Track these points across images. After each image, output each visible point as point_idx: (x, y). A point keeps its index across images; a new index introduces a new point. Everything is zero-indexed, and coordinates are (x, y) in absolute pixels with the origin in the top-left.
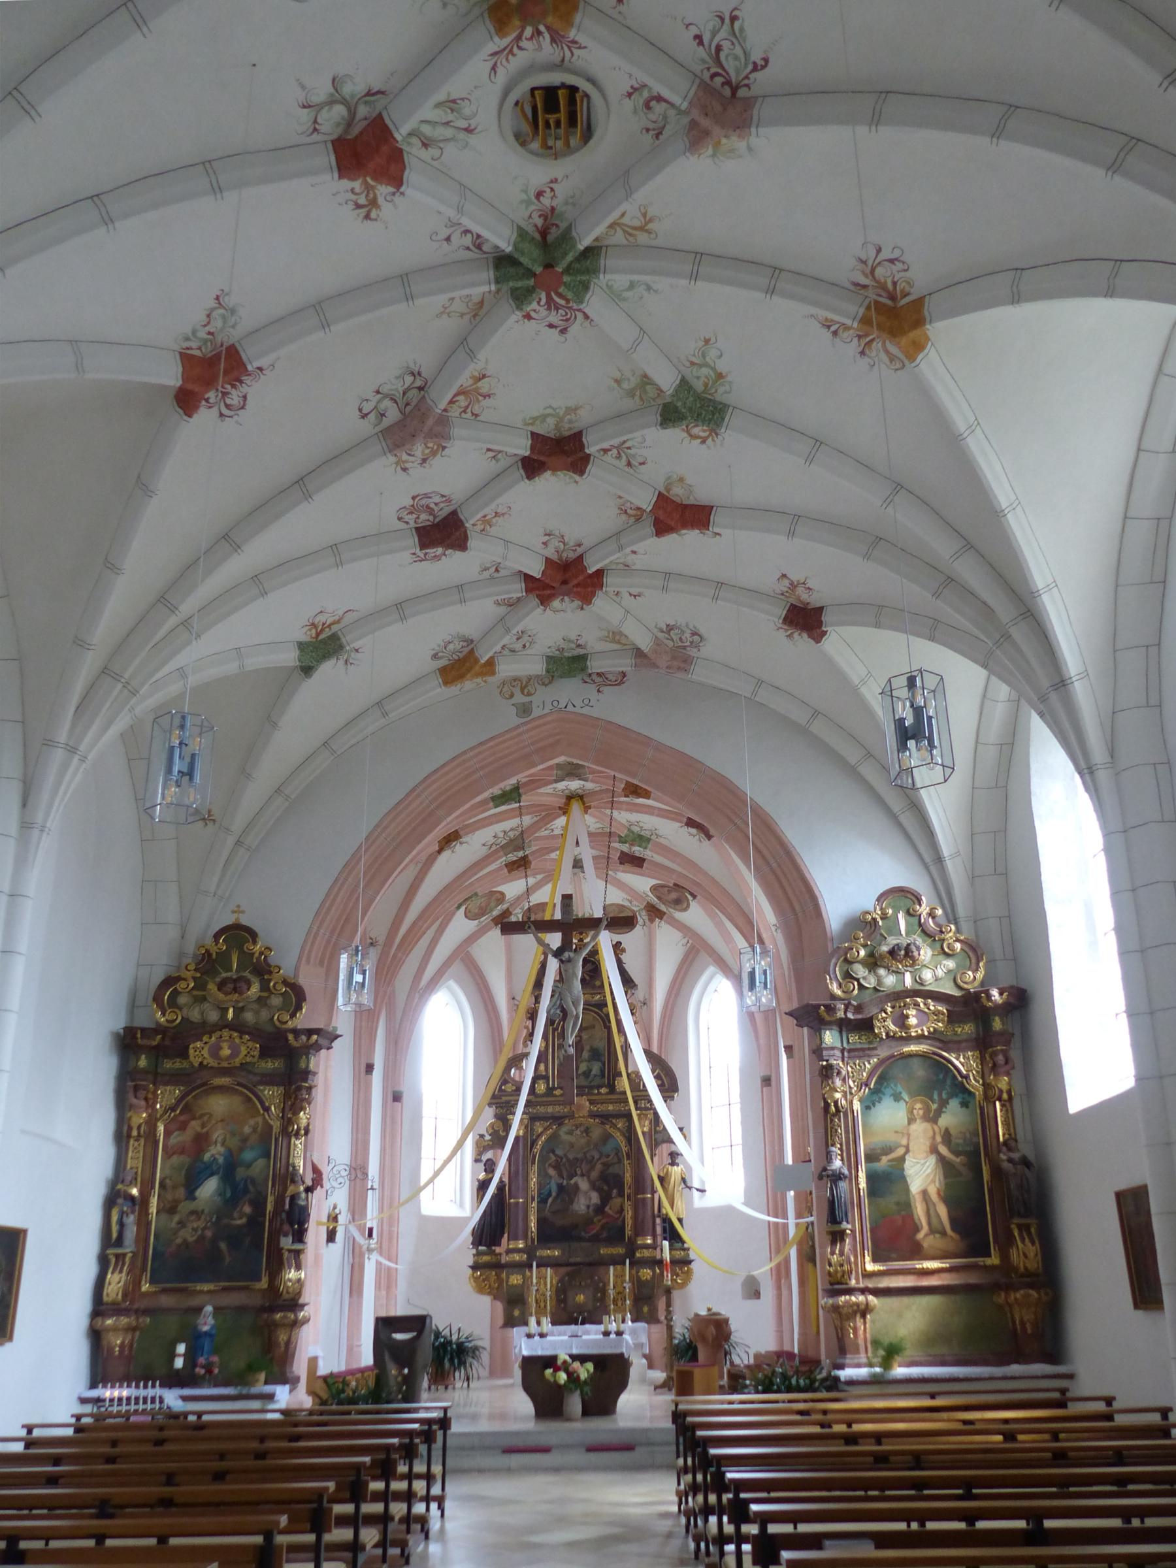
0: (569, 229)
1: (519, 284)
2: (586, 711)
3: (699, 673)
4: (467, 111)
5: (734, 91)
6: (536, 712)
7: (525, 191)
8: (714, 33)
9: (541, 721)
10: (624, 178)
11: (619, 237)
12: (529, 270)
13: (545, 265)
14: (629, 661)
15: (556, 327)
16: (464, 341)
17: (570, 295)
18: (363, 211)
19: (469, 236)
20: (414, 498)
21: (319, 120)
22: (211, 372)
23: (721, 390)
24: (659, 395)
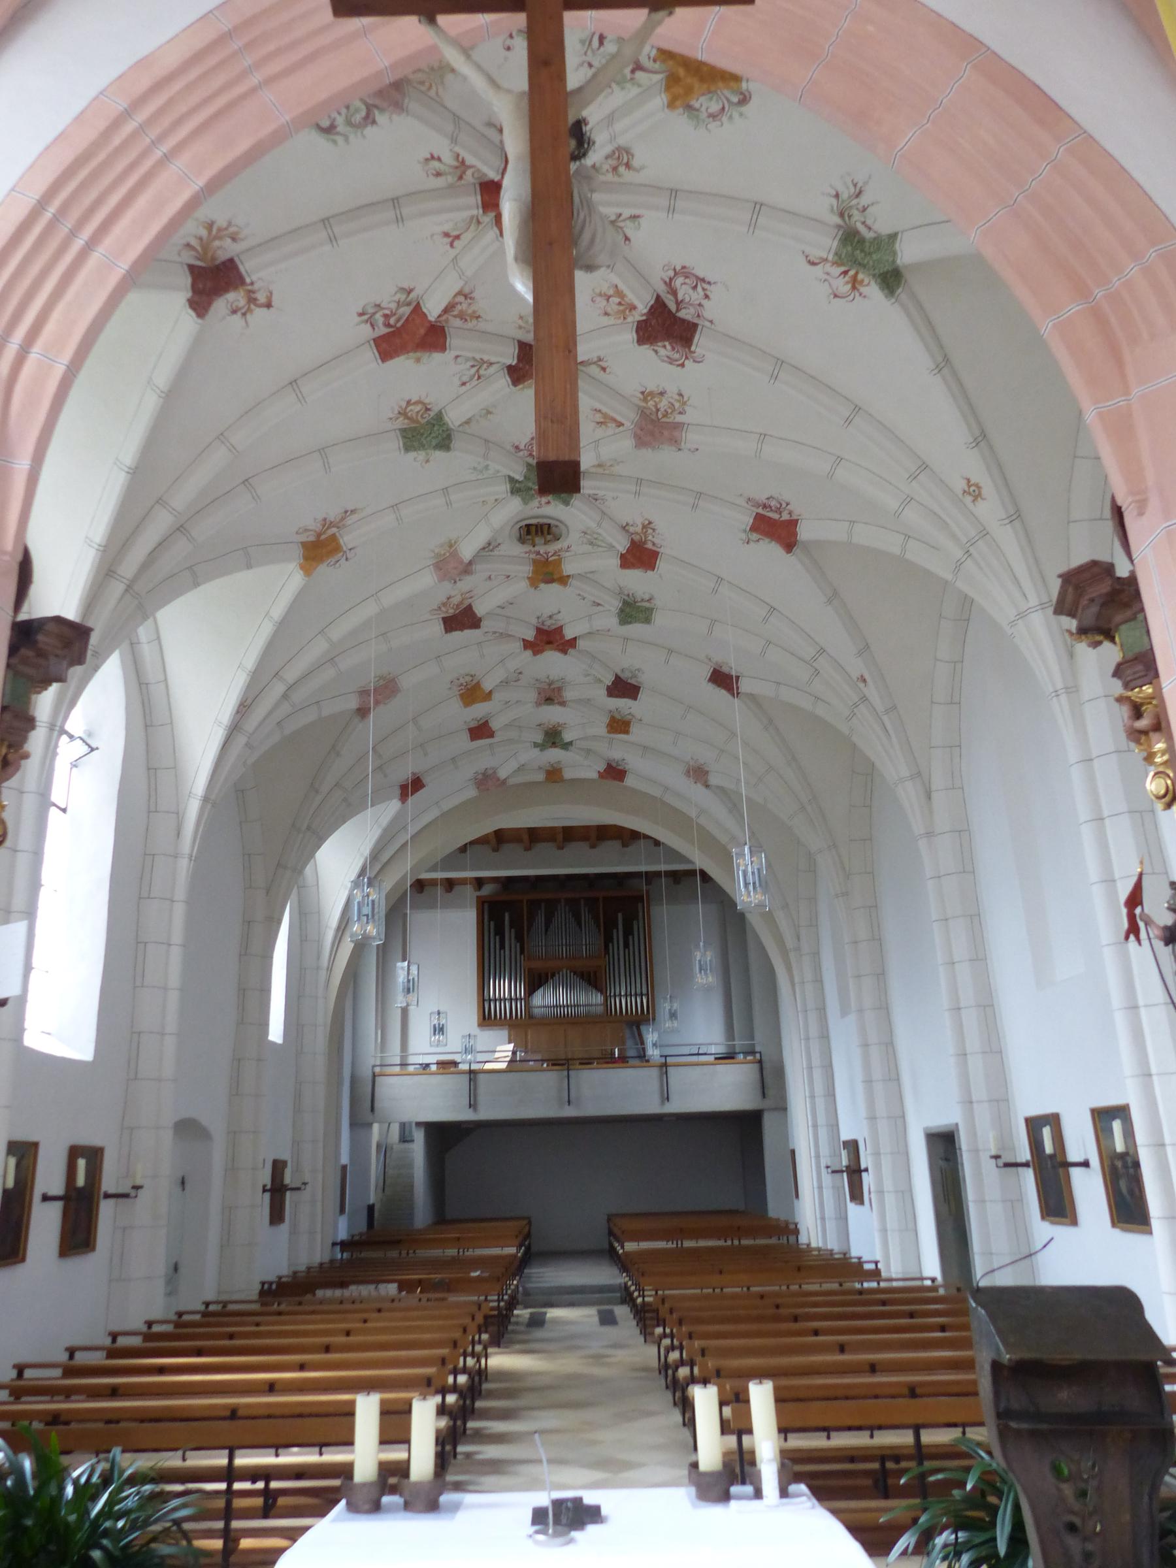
20: (683, 365)
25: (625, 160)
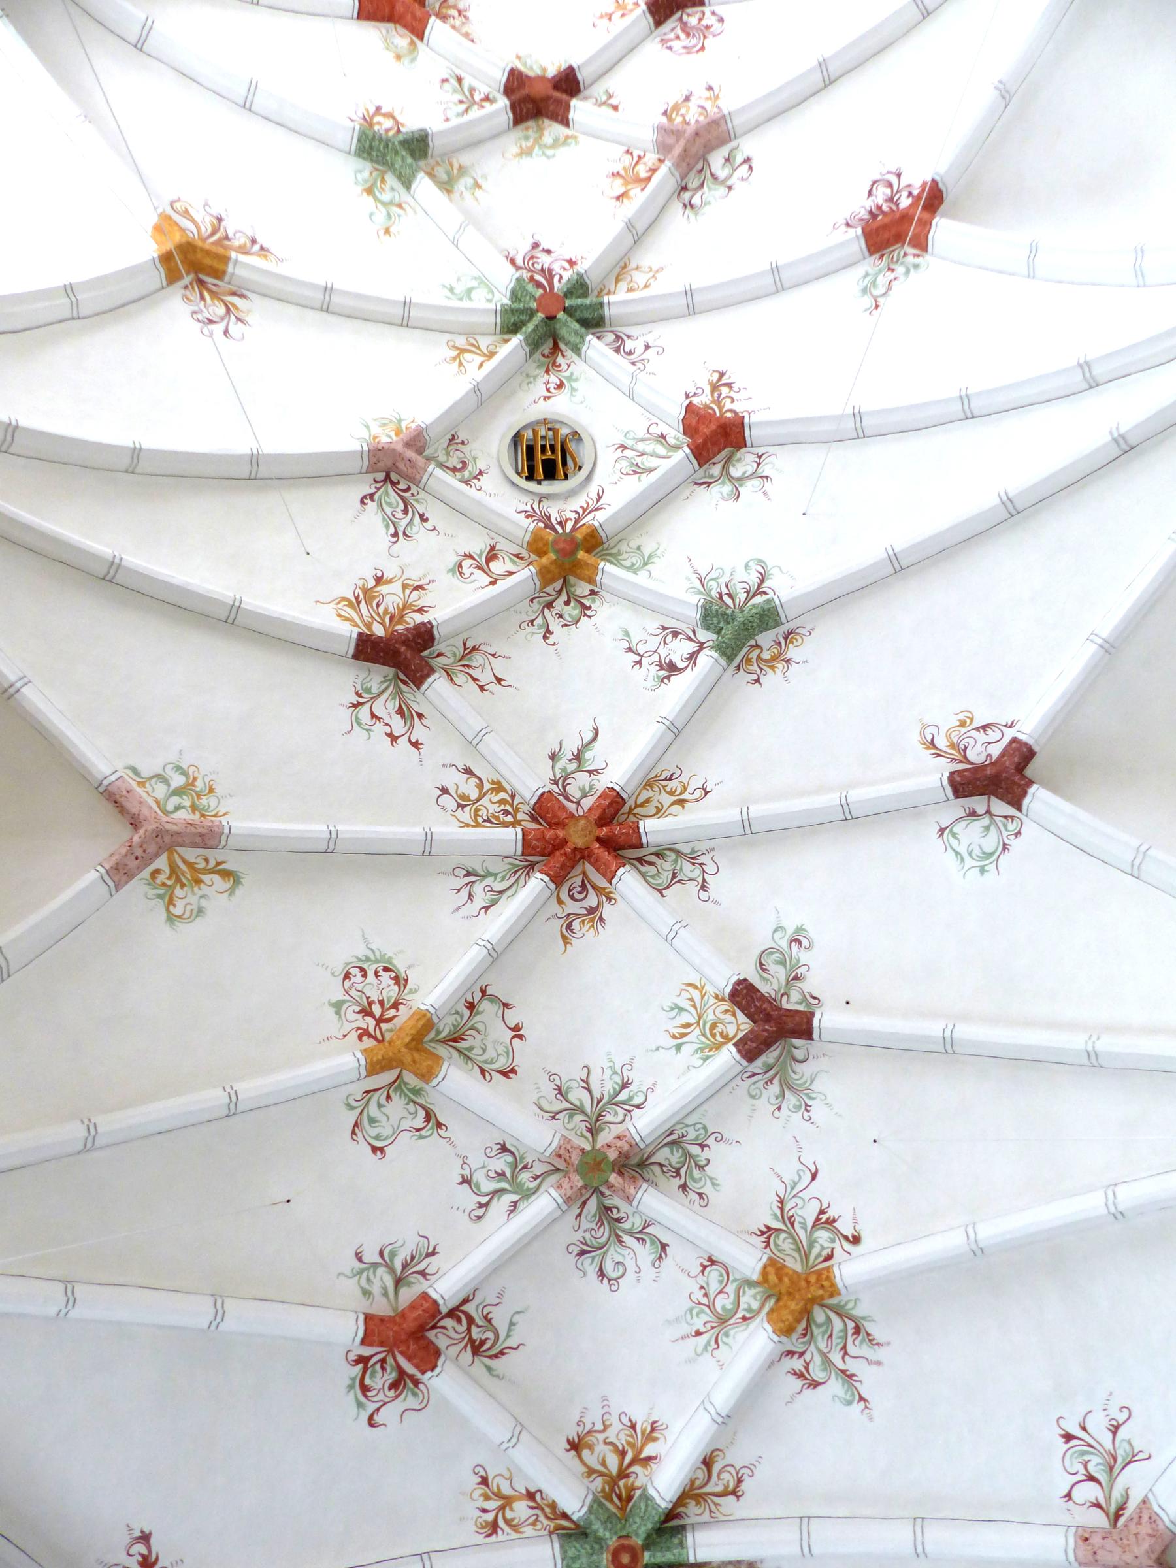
0: (531, 354)
1: (579, 301)
4: (624, 464)
5: (388, 478)
7: (573, 389)
8: (411, 522)
10: (482, 401)
11: (484, 342)
12: (570, 315)
13: (555, 317)
15: (543, 250)
16: (638, 240)
17: (530, 287)
18: (725, 380)
19: (627, 350)
20: (200, 911)
21: (755, 465)
22: (894, 231)
23: (366, 174)
24: (433, 169)
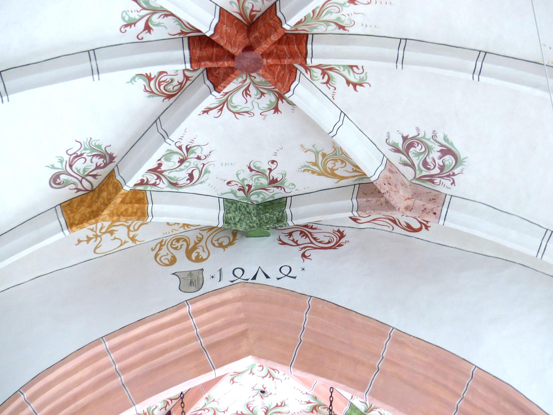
2: (286, 283)
3: (456, 220)
6: (209, 285)
9: (215, 299)
14: (348, 203)
25: (152, 83)
